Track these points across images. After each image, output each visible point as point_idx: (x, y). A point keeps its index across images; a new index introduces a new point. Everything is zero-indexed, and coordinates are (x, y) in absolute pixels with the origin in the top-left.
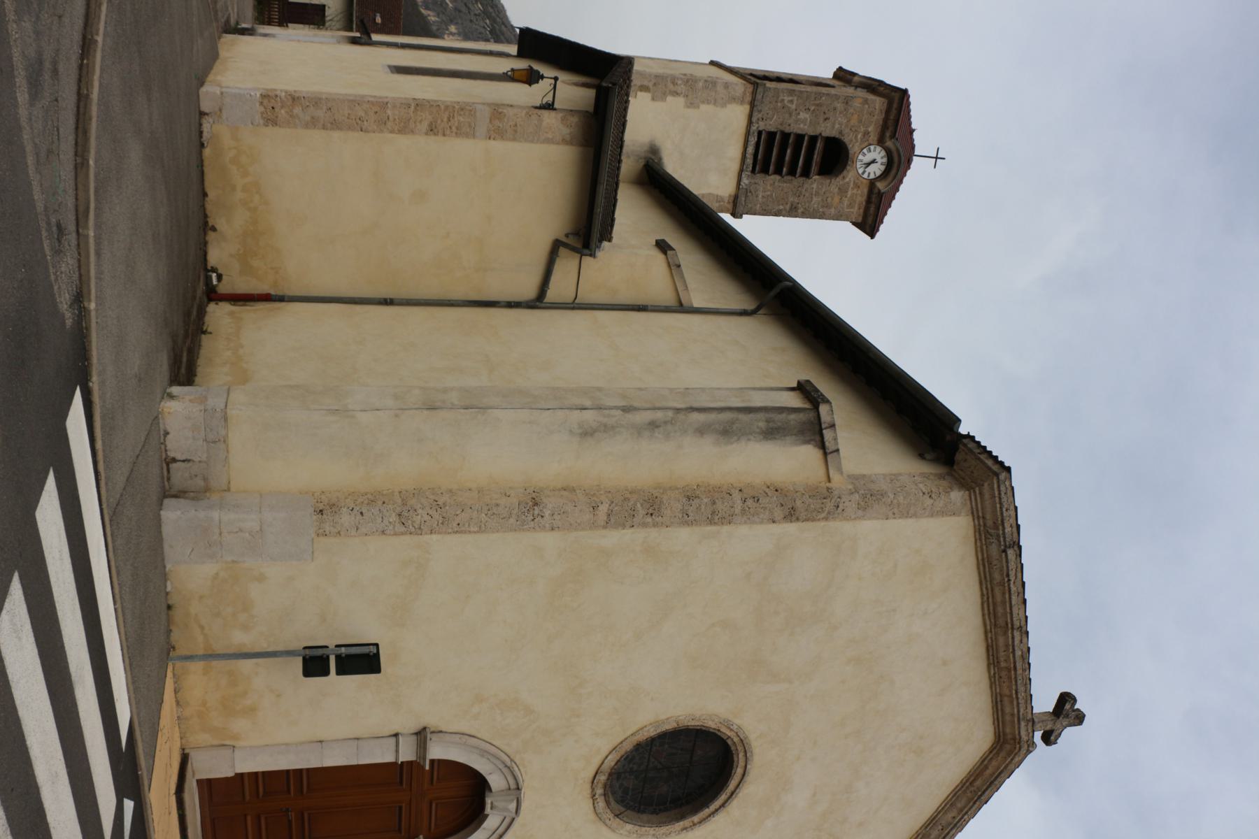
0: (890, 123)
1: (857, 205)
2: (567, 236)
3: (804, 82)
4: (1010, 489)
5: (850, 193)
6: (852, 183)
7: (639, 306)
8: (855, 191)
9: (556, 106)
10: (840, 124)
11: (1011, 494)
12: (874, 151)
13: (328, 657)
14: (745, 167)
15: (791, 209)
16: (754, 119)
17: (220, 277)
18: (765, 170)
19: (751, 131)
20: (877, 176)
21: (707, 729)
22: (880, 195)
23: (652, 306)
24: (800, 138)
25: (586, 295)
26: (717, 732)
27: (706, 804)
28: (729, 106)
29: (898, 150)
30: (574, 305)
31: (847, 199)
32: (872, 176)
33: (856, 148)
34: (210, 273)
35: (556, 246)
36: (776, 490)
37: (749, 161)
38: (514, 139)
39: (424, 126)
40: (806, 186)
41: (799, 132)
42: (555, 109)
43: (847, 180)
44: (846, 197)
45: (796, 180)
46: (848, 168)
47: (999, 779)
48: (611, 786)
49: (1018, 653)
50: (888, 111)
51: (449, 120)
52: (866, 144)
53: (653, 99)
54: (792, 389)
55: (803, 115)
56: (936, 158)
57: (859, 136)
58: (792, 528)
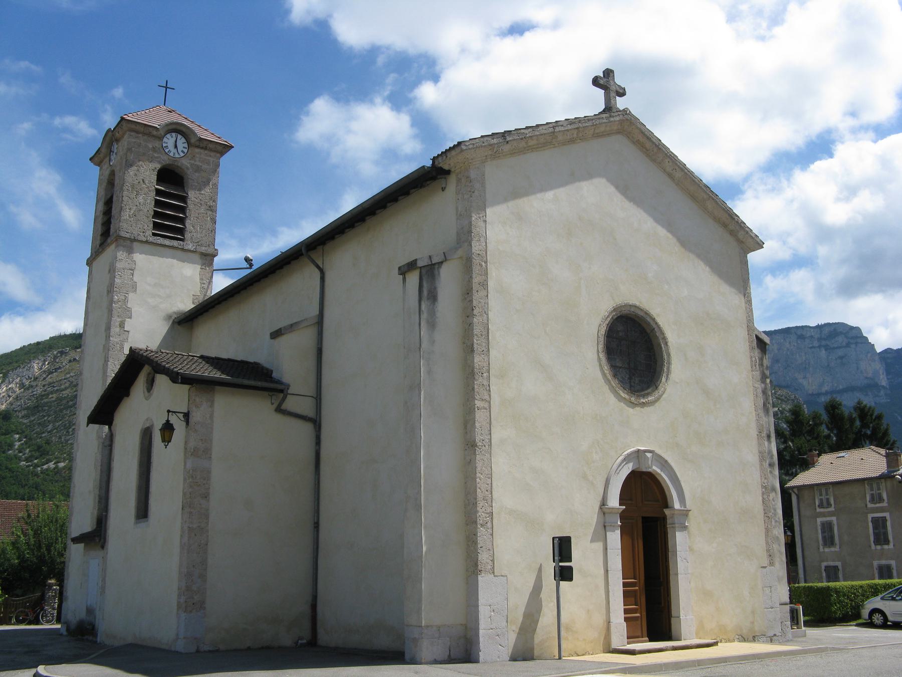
1: (207, 158)
2: (272, 404)
3: (109, 197)
4: (471, 141)
5: (198, 163)
6: (191, 161)
7: (318, 353)
8: (197, 159)
9: (186, 411)
11: (473, 140)
12: (167, 143)
13: (561, 566)
14: (180, 247)
15: (211, 210)
16: (144, 239)
17: (301, 638)
18: (181, 231)
20: (185, 141)
21: (607, 332)
23: (318, 345)
24: (158, 203)
25: (312, 391)
26: (609, 326)
30: (318, 398)
31: (203, 166)
32: (186, 145)
33: (166, 158)
34: (299, 644)
35: (279, 410)
36: (468, 294)
37: (175, 243)
42: (189, 412)
44: (201, 166)
45: (189, 206)
47: (646, 133)
48: (638, 391)
49: (569, 127)
51: (200, 485)
52: (162, 150)
53: (130, 318)
54: (404, 280)
56: (166, 88)
57: (156, 155)
58: (491, 284)
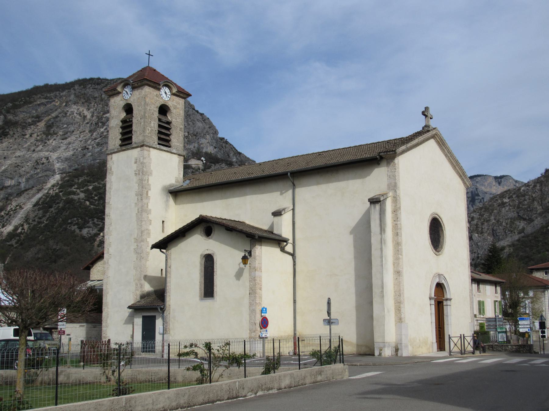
0: (154, 85)
5: (175, 104)
10: (154, 107)
18: (168, 141)
19: (159, 148)
22: (178, 91)
27: (439, 222)
28: (151, 157)
29: (165, 82)
33: (161, 100)
37: (165, 148)
38: (261, 264)
39: (260, 291)
40: (174, 124)
41: (157, 127)
43: (171, 105)
46: (167, 105)
50: (150, 86)
55: (152, 125)
